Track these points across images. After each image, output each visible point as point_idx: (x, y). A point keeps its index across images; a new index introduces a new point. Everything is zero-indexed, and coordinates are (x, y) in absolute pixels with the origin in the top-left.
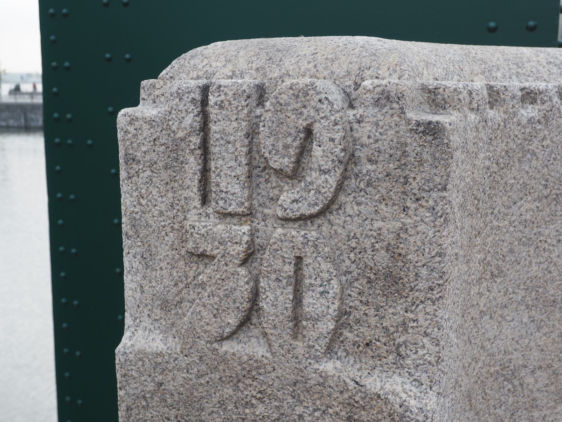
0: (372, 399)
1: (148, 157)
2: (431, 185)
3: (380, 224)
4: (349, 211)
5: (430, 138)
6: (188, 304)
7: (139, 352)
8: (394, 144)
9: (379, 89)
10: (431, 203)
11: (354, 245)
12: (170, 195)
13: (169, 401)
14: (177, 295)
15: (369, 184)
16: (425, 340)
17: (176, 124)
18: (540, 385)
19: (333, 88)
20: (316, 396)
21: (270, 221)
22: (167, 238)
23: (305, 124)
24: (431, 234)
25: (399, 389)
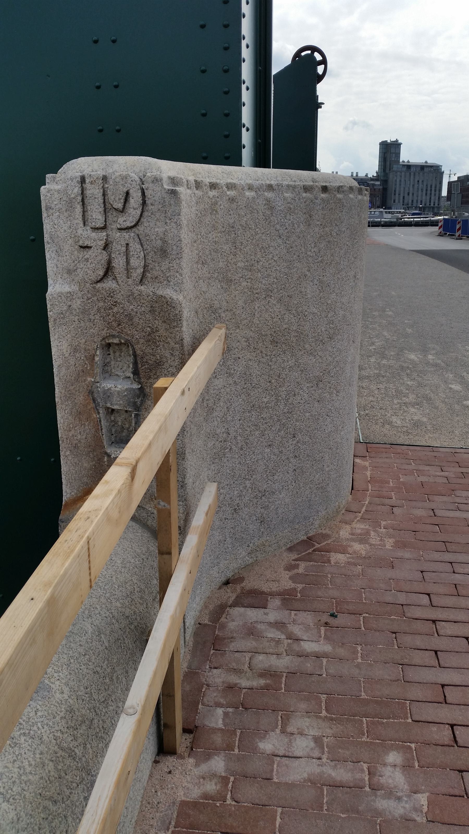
0: (159, 297)
1: (57, 207)
2: (175, 213)
3: (156, 230)
4: (145, 225)
5: (173, 195)
6: (80, 270)
7: (59, 293)
8: (160, 198)
9: (153, 177)
10: (175, 220)
11: (148, 238)
12: (69, 222)
13: (74, 313)
14: (74, 267)
15: (152, 214)
16: (177, 274)
17: (71, 191)
18: (227, 318)
19: (136, 177)
20: (138, 300)
21: (114, 231)
22: (68, 242)
23: (126, 190)
24: (176, 232)
25: (169, 293)
